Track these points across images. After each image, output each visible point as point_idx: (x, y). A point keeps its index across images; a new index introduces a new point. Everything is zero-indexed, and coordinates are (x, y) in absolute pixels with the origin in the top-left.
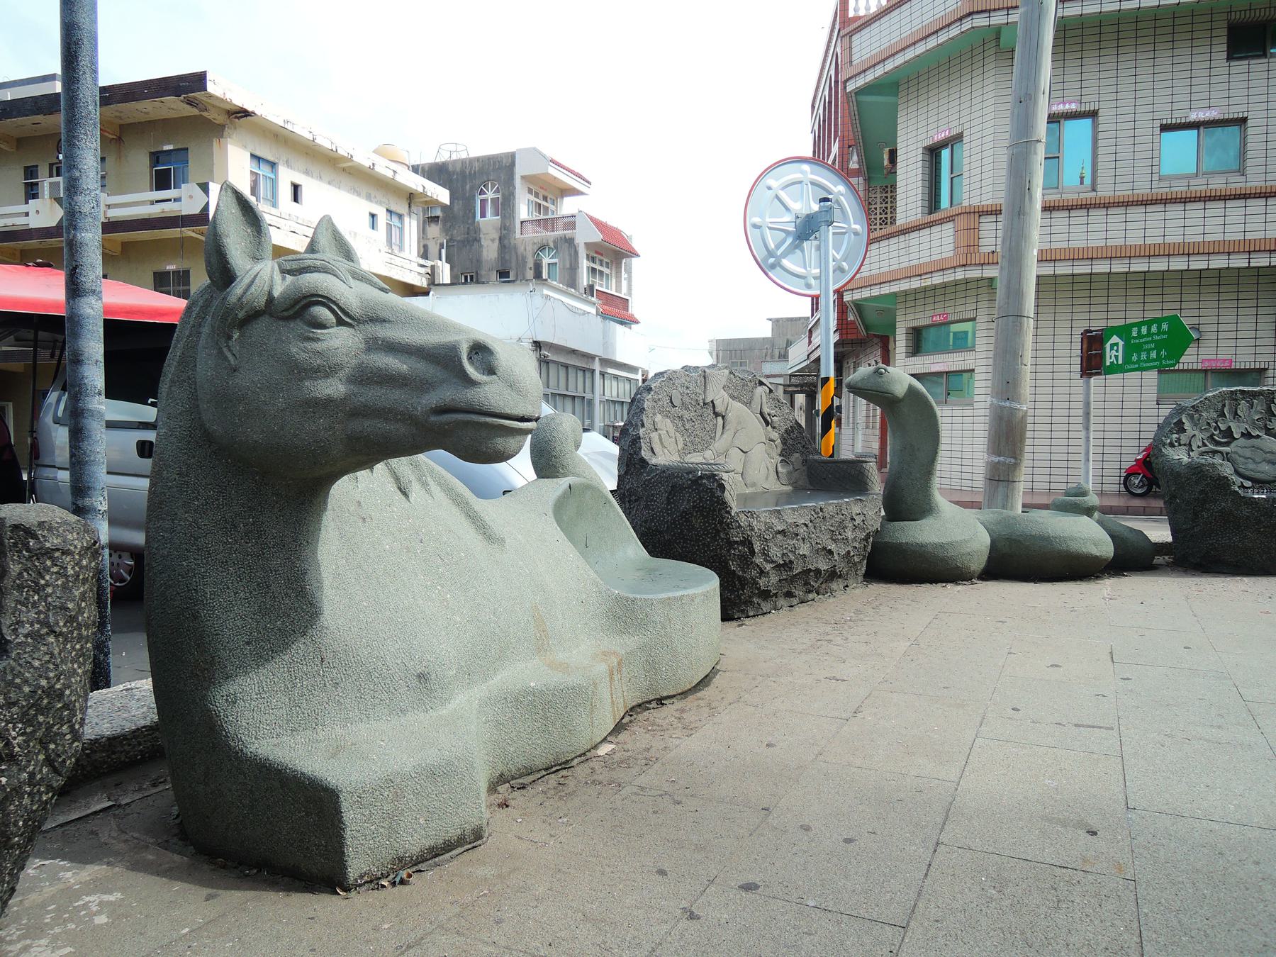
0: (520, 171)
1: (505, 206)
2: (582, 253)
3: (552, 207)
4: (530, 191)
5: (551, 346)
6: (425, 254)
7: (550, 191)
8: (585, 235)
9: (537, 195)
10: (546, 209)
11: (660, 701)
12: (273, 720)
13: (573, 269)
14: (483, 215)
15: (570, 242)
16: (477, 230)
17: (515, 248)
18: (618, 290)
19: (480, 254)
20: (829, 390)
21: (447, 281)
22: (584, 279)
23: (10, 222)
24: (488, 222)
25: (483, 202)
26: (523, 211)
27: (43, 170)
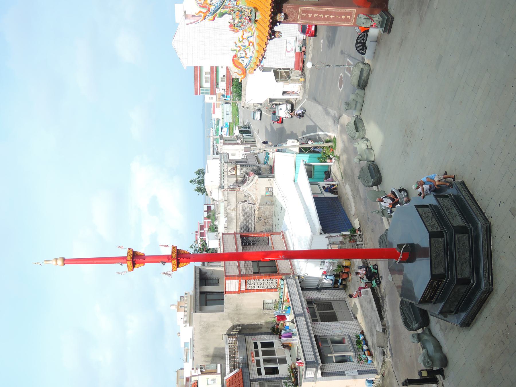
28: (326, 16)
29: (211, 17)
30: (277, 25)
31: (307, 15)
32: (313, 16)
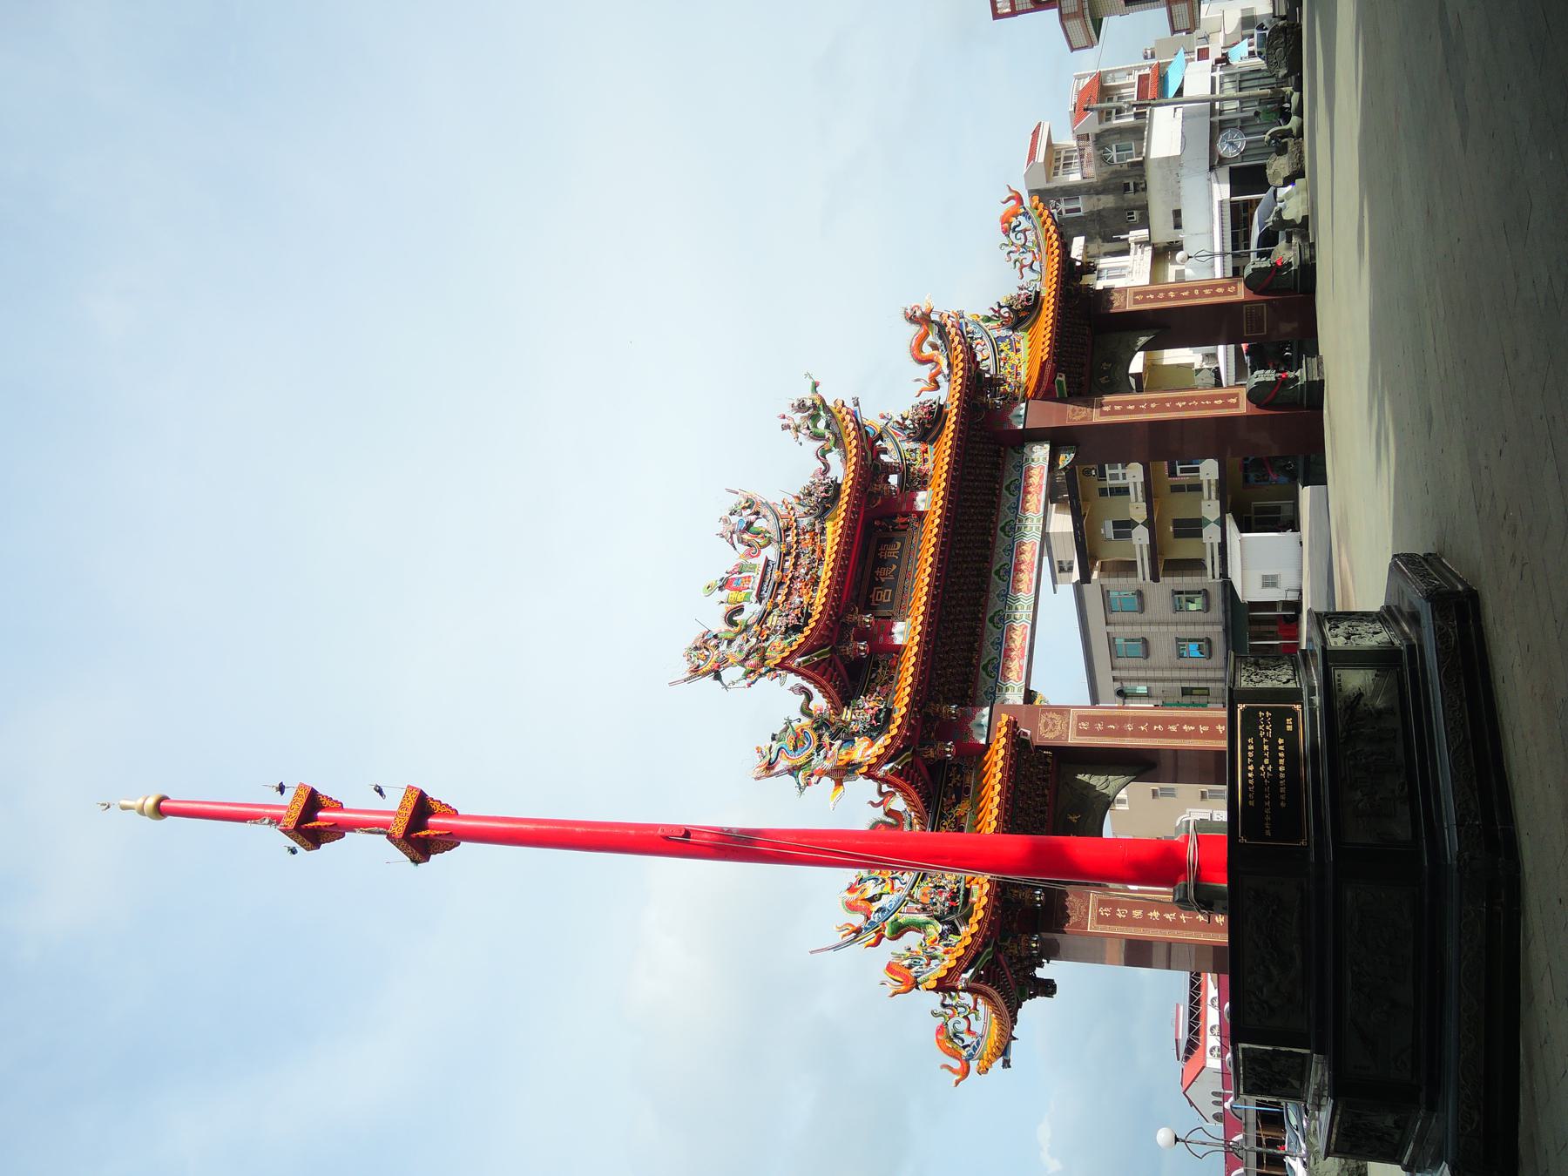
0: (1043, 185)
1: (1070, 192)
2: (1106, 125)
3: (1063, 154)
4: (1056, 174)
5: (1211, 160)
6: (1126, 252)
7: (1057, 159)
8: (1091, 123)
9: (1057, 168)
10: (1066, 158)
11: (423, 831)
12: (1299, 221)
13: (1120, 131)
14: (1078, 210)
15: (1098, 137)
16: (1091, 213)
17: (1104, 181)
18: (1132, 85)
19: (1110, 210)
20: (1261, 224)
21: (1146, 232)
22: (1128, 120)
23: (1140, 494)
24: (1083, 205)
25: (1068, 211)
26: (1075, 177)
27: (1102, 485)
28: (1168, 916)
29: (872, 936)
30: (1041, 965)
31: (1113, 913)
32: (1130, 915)
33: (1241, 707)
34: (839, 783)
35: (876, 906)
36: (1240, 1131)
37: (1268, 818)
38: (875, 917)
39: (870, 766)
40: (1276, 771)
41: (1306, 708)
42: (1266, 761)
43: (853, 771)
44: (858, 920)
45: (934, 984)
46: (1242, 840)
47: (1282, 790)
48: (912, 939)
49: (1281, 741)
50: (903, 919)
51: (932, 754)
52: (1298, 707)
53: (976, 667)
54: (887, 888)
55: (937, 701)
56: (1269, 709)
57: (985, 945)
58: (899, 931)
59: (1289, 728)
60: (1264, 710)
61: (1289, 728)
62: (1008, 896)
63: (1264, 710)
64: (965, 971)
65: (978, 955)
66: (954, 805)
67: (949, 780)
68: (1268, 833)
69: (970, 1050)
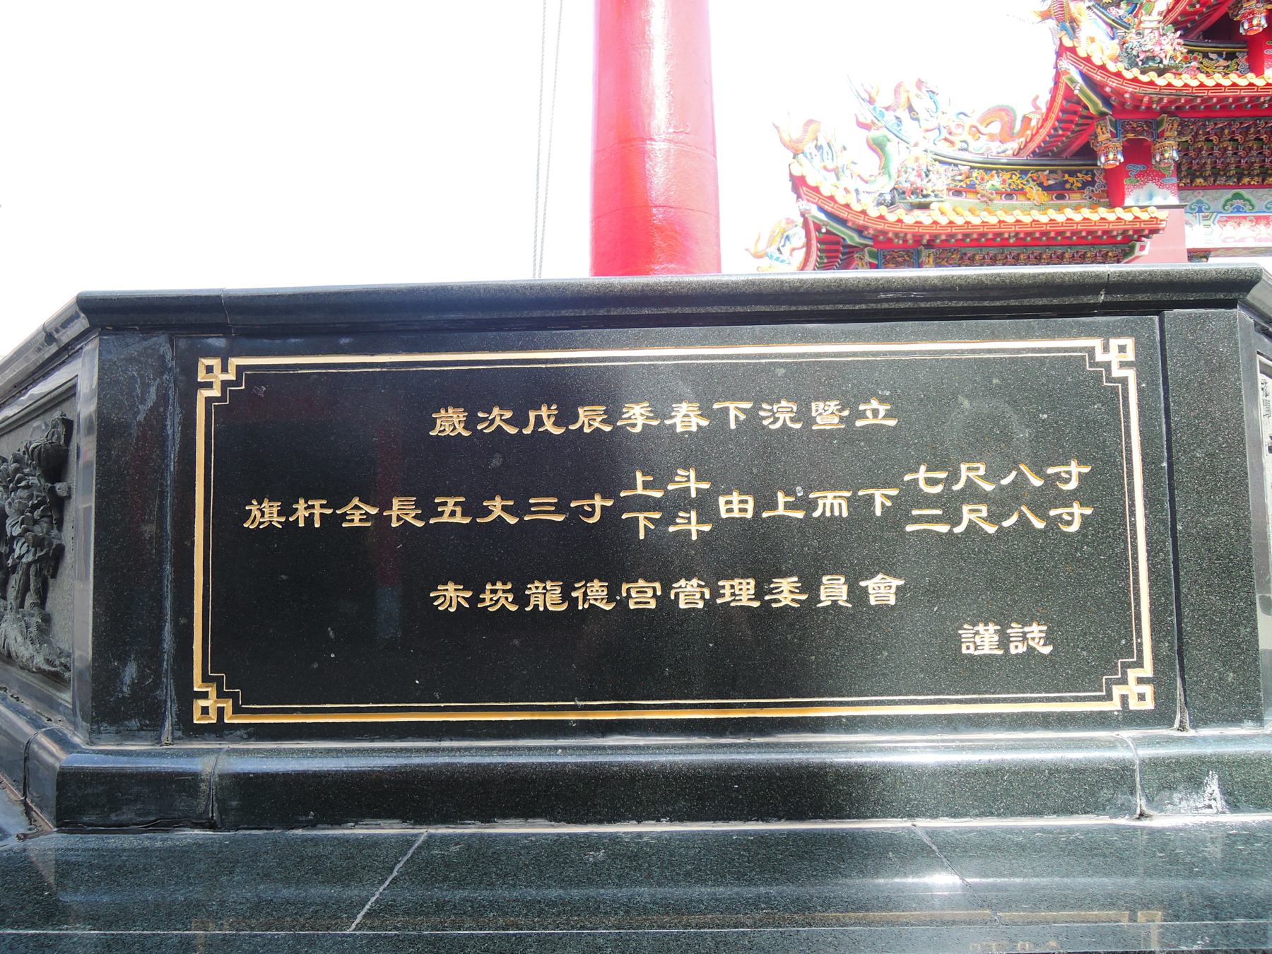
29: (867, 118)
33: (1115, 352)
34: (1045, 16)
35: (904, 115)
36: (764, 520)
37: (357, 513)
38: (889, 117)
39: (1073, 50)
40: (666, 562)
41: (1129, 747)
42: (736, 506)
43: (1064, 28)
44: (885, 99)
45: (797, 173)
46: (216, 375)
47: (546, 596)
48: (870, 162)
49: (882, 589)
50: (891, 148)
51: (1101, 138)
52: (1136, 690)
53: (1238, 185)
54: (925, 125)
55: (1180, 134)
56: (1109, 521)
57: (860, 231)
58: (878, 147)
59: (981, 640)
60: (1104, 489)
61: (981, 640)
62: (925, 252)
63: (1104, 489)
64: (821, 209)
65: (843, 222)
66: (1041, 185)
67: (1072, 174)
68: (264, 514)
69: (777, 254)
